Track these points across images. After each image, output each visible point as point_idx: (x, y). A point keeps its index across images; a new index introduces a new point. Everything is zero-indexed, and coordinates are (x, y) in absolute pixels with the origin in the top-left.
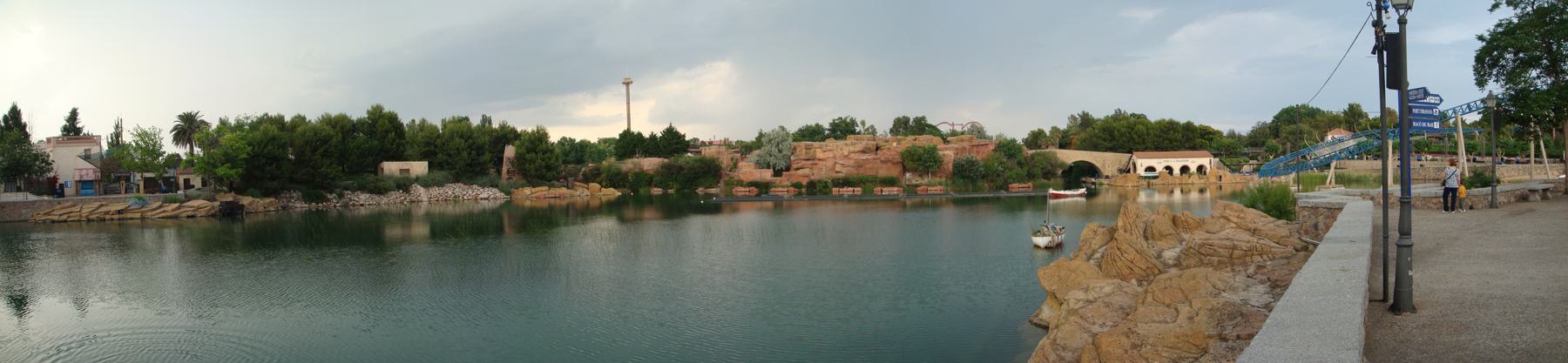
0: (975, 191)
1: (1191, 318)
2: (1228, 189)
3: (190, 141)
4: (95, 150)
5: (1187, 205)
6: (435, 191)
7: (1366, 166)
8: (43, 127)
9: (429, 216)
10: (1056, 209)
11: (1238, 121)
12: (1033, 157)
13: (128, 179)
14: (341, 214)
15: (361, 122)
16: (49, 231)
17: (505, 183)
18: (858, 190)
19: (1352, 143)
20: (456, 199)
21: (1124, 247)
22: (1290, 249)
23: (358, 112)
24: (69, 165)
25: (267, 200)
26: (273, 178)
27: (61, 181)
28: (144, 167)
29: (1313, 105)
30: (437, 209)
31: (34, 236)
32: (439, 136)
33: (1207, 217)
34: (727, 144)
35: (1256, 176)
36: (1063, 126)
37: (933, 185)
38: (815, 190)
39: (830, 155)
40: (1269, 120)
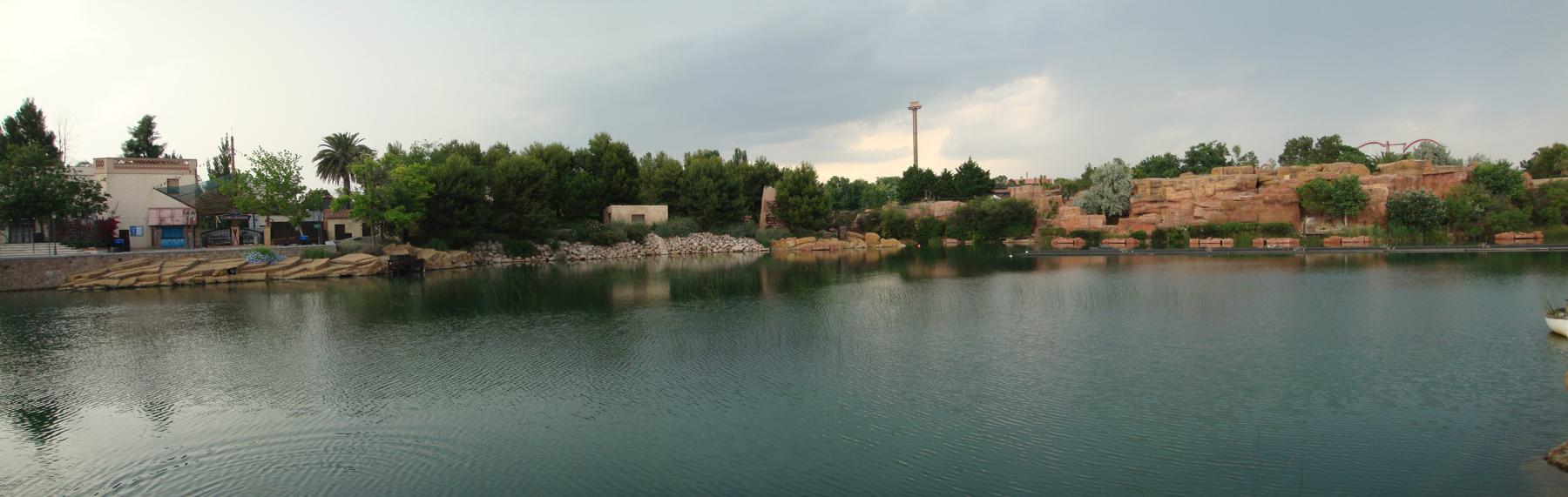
0: (1426, 244)
3: (344, 173)
4: (185, 181)
6: (677, 242)
8: (86, 139)
9: (669, 273)
12: (1543, 190)
13: (244, 224)
15: (581, 155)
16: (100, 302)
17: (764, 232)
18: (1228, 242)
20: (703, 253)
23: (577, 142)
24: (136, 201)
25: (456, 254)
26: (465, 226)
27: (121, 227)
28: (270, 208)
30: (678, 264)
31: (69, 312)
32: (681, 174)
34: (1044, 183)
38: (1164, 242)
39: (1187, 194)
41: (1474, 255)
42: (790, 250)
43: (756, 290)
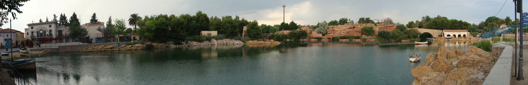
0: (389, 43)
1: (461, 84)
2: (472, 42)
3: (135, 24)
4: (102, 27)
5: (460, 47)
7: (510, 36)
9: (217, 50)
10: (417, 48)
11: (475, 21)
12: (410, 31)
13: (114, 37)
14: (187, 49)
15: (194, 17)
18: (348, 40)
19: (507, 29)
20: (227, 44)
21: (440, 61)
22: (490, 61)
23: (193, 13)
24: (93, 33)
25: (162, 44)
27: (91, 38)
28: (119, 33)
29: (497, 17)
30: (220, 47)
32: (221, 22)
33: (466, 51)
34: (309, 26)
35: (481, 38)
36: (420, 20)
37: (371, 39)
38: (335, 40)
40: (485, 21)
41: (397, 45)
42: (250, 44)
43: (241, 55)
